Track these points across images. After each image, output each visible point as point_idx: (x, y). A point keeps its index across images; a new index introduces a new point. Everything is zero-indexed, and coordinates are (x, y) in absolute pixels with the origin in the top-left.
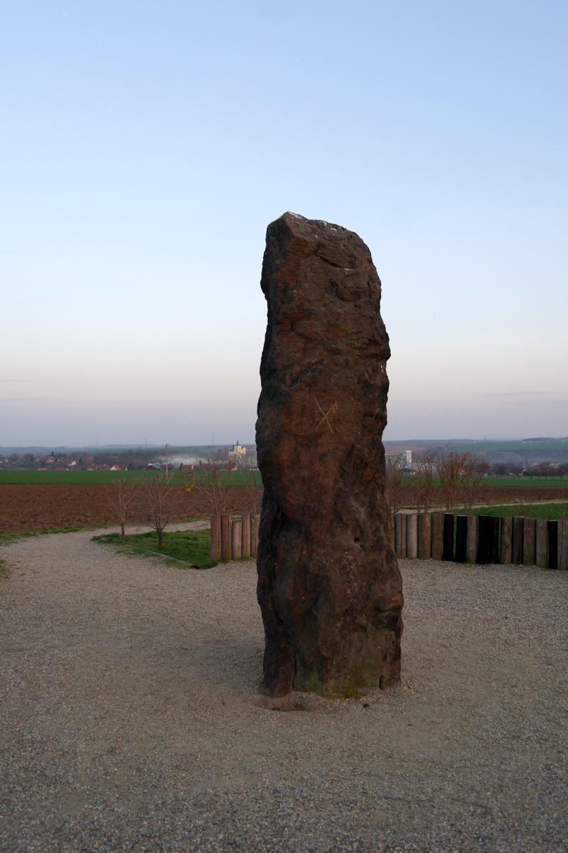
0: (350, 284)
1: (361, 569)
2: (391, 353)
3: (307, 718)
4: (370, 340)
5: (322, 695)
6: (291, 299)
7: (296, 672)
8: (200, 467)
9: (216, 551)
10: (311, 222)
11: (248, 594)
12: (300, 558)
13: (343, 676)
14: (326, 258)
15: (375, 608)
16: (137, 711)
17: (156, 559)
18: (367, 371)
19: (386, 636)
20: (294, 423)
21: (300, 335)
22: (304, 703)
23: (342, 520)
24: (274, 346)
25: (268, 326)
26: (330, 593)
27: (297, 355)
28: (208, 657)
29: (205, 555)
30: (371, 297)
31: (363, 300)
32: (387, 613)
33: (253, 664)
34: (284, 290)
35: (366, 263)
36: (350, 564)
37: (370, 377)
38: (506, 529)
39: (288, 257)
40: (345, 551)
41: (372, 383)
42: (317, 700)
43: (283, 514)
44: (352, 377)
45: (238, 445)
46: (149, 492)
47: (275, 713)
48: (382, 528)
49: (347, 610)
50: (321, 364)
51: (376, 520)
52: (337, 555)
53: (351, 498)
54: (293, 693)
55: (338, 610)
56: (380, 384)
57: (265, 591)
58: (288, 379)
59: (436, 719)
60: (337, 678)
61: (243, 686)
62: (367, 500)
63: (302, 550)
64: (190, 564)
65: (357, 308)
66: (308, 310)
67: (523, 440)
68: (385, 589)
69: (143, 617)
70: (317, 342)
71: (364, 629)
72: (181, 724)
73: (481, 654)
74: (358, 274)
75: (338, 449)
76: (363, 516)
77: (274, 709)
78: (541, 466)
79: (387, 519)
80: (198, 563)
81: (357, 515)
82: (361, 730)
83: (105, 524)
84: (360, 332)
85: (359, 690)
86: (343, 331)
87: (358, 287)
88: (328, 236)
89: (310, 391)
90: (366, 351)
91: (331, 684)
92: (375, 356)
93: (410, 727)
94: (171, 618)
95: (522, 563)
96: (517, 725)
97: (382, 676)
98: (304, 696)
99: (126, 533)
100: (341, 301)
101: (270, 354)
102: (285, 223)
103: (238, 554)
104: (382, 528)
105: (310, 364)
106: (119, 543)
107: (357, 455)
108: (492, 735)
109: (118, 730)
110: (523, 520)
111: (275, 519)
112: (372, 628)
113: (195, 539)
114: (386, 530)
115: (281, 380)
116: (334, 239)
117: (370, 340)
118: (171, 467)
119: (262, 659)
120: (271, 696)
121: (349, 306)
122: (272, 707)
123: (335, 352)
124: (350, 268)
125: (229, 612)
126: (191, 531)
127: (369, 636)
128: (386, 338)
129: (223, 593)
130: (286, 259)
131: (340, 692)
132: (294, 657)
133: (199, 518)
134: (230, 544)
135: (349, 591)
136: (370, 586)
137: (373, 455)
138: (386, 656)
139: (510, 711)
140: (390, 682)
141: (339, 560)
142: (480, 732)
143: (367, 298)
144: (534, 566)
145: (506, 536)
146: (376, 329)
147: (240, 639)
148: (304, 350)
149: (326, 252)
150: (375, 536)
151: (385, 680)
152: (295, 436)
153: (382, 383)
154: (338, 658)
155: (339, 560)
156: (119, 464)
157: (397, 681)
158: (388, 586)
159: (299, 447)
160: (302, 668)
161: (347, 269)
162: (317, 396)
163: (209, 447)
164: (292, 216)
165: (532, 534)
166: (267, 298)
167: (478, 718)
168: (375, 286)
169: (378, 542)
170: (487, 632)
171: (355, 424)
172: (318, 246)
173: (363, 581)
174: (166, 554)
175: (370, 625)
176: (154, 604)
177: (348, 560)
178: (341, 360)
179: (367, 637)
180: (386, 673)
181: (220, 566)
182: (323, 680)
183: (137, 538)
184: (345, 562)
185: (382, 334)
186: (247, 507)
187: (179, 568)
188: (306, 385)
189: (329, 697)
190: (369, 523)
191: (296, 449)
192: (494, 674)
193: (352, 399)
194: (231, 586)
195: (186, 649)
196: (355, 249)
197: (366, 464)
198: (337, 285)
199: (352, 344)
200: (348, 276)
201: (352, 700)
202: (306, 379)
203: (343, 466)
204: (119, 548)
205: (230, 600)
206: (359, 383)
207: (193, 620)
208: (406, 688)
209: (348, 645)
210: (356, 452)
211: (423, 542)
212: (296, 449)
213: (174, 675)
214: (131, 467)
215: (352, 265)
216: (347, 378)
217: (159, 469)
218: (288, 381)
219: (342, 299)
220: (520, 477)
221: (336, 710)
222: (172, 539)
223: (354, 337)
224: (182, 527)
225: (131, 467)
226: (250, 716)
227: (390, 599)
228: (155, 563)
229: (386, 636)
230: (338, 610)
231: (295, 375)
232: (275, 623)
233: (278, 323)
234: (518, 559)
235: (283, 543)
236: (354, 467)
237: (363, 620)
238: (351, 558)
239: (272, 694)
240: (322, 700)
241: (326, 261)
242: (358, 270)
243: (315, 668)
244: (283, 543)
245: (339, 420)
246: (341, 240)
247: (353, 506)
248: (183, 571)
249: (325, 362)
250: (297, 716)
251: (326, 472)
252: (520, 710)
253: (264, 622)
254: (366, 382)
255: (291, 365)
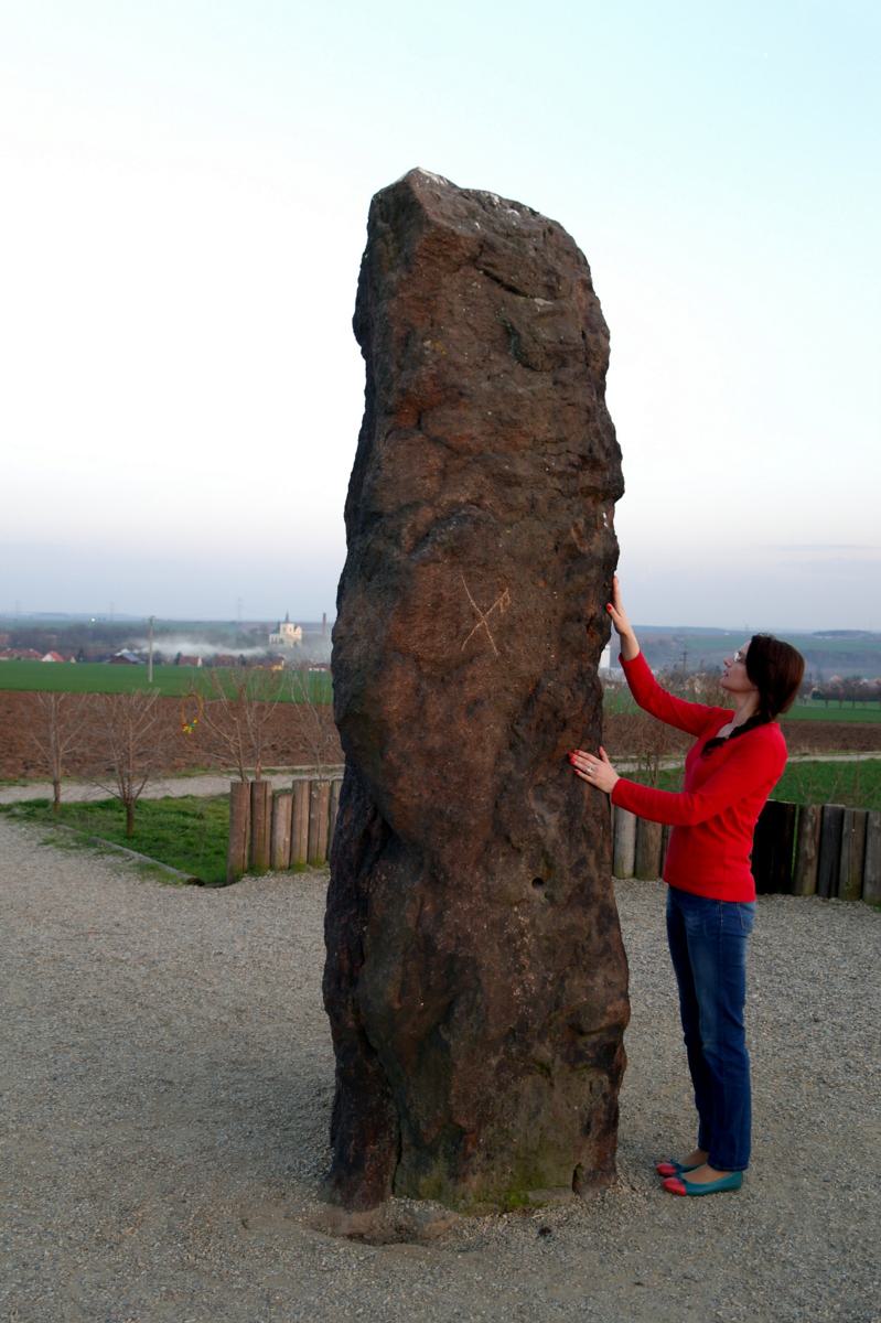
0: (545, 334)
1: (545, 943)
2: (626, 487)
3: (423, 1263)
4: (582, 457)
5: (455, 1207)
6: (419, 360)
7: (399, 1156)
8: (214, 662)
9: (239, 852)
10: (467, 194)
11: (300, 951)
12: (418, 923)
13: (499, 1168)
14: (496, 273)
15: (570, 1026)
16: (56, 1242)
17: (119, 860)
18: (576, 525)
19: (591, 1083)
20: (416, 632)
21: (436, 440)
22: (416, 1224)
23: (508, 839)
24: (379, 462)
25: (365, 416)
26: (479, 996)
27: (428, 483)
28: (216, 1104)
29: (217, 853)
30: (588, 365)
31: (571, 370)
32: (594, 1038)
33: (308, 1123)
34: (405, 342)
35: (580, 291)
36: (522, 934)
37: (581, 537)
38: (809, 828)
39: (415, 268)
40: (512, 905)
41: (582, 549)
42: (443, 1218)
43: (385, 826)
44: (542, 537)
45: (287, 621)
46: (111, 724)
47: (357, 1251)
48: (591, 859)
49: (512, 1031)
50: (478, 505)
51: (579, 841)
52: (496, 915)
53: (530, 792)
54: (393, 1200)
55: (493, 1031)
56: (600, 554)
57: (342, 984)
58: (408, 537)
59: (692, 1270)
60: (486, 1172)
61: (287, 1178)
62: (561, 798)
63: (422, 905)
64: (187, 877)
65: (559, 387)
66: (454, 386)
67: (816, 634)
68: (592, 988)
69: (85, 1002)
70: (471, 459)
71: (546, 1070)
72: (152, 1276)
73: (773, 1107)
74: (563, 313)
75: (506, 689)
76: (553, 832)
77: (351, 1237)
78: (846, 682)
79: (604, 839)
80: (203, 876)
81: (541, 831)
82: (535, 1295)
83: (23, 776)
84: (565, 440)
85: (530, 1194)
86: (526, 435)
87: (561, 342)
88: (502, 225)
89: (452, 565)
90: (573, 481)
91: (474, 1184)
92: (592, 492)
93: (639, 1288)
94: (141, 1004)
95: (836, 896)
96: (861, 1288)
97: (579, 1166)
98: (416, 1209)
99: (63, 799)
100: (526, 371)
101: (368, 477)
102: (412, 193)
103: (282, 858)
104: (591, 859)
105: (455, 505)
106: (47, 821)
107: (545, 704)
108: (811, 1314)
109: (12, 1294)
110: (843, 811)
111: (367, 834)
112: (561, 1068)
113: (200, 817)
114: (599, 864)
115: (390, 538)
116: (510, 234)
117: (582, 457)
118: (158, 659)
119: (328, 1113)
120: (347, 1209)
121: (542, 383)
122: (348, 1231)
123: (510, 481)
124: (546, 300)
125: (262, 993)
126: (193, 797)
127: (556, 1083)
128: (615, 453)
129: (252, 949)
130: (410, 272)
131: (492, 1201)
132: (398, 1125)
133: (207, 770)
134: (268, 839)
135: (518, 992)
136: (562, 980)
137: (581, 702)
138: (588, 1126)
139: (844, 1251)
140: (595, 1179)
141: (498, 926)
142: (785, 1305)
143: (580, 367)
144: (858, 903)
145: (807, 842)
146: (597, 433)
147: (283, 1059)
148: (444, 474)
149: (496, 261)
150: (576, 876)
151: (584, 1173)
152: (417, 659)
153: (604, 549)
154: (491, 1131)
155: (498, 926)
156: (59, 650)
157: (609, 1175)
158: (599, 980)
159: (424, 685)
160: (413, 1150)
161: (540, 301)
162: (468, 574)
163: (233, 623)
164: (427, 177)
165: (860, 840)
166: (366, 354)
167: (778, 1268)
168: (597, 342)
169: (581, 887)
170: (782, 1053)
171: (544, 638)
172: (481, 247)
173: (548, 969)
174: (139, 851)
175: (558, 1062)
176: (108, 973)
177: (518, 925)
178: (521, 499)
179: (552, 1085)
180: (587, 1161)
181: (247, 883)
182: (456, 1175)
183: (86, 808)
184: (512, 930)
185: (607, 445)
186: (301, 747)
187: (165, 884)
188: (445, 552)
189: (468, 1211)
190: (564, 848)
191: (417, 689)
192: (802, 1154)
193: (541, 584)
194: (267, 930)
195: (171, 1083)
196: (558, 258)
197: (565, 723)
198: (519, 335)
199: (546, 465)
200: (542, 315)
201: (516, 1217)
202: (445, 537)
203: (516, 727)
204: (46, 832)
205: (264, 965)
206: (556, 549)
207: (188, 1013)
208: (626, 1190)
209: (511, 1103)
210: (543, 697)
211: (646, 846)
212: (417, 689)
213: (141, 1148)
214: (81, 655)
215: (551, 292)
216: (532, 537)
217: (135, 663)
218: (407, 540)
219: (526, 365)
220: (805, 700)
221: (482, 1244)
222: (154, 814)
223: (552, 449)
224: (178, 788)
225: (81, 655)
226: (300, 1256)
227: (604, 1008)
228: (117, 871)
229: (591, 1083)
230: (493, 1031)
231: (420, 528)
232: (359, 1053)
233: (389, 413)
234: (830, 887)
235: (383, 888)
236: (538, 727)
237: (544, 1051)
238: (525, 920)
239: (347, 1203)
240: (454, 1217)
241: (498, 280)
242: (563, 303)
243: (441, 1148)
244: (383, 888)
245: (511, 628)
246: (529, 236)
247: (533, 811)
248: (171, 890)
249: (487, 502)
250: (399, 1259)
251: (481, 739)
252: (864, 1250)
253: (329, 921)
254: (572, 547)
255: (414, 506)
